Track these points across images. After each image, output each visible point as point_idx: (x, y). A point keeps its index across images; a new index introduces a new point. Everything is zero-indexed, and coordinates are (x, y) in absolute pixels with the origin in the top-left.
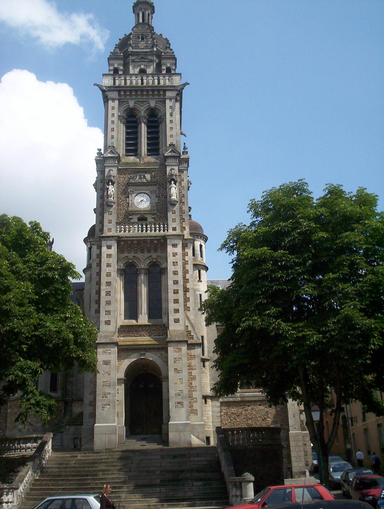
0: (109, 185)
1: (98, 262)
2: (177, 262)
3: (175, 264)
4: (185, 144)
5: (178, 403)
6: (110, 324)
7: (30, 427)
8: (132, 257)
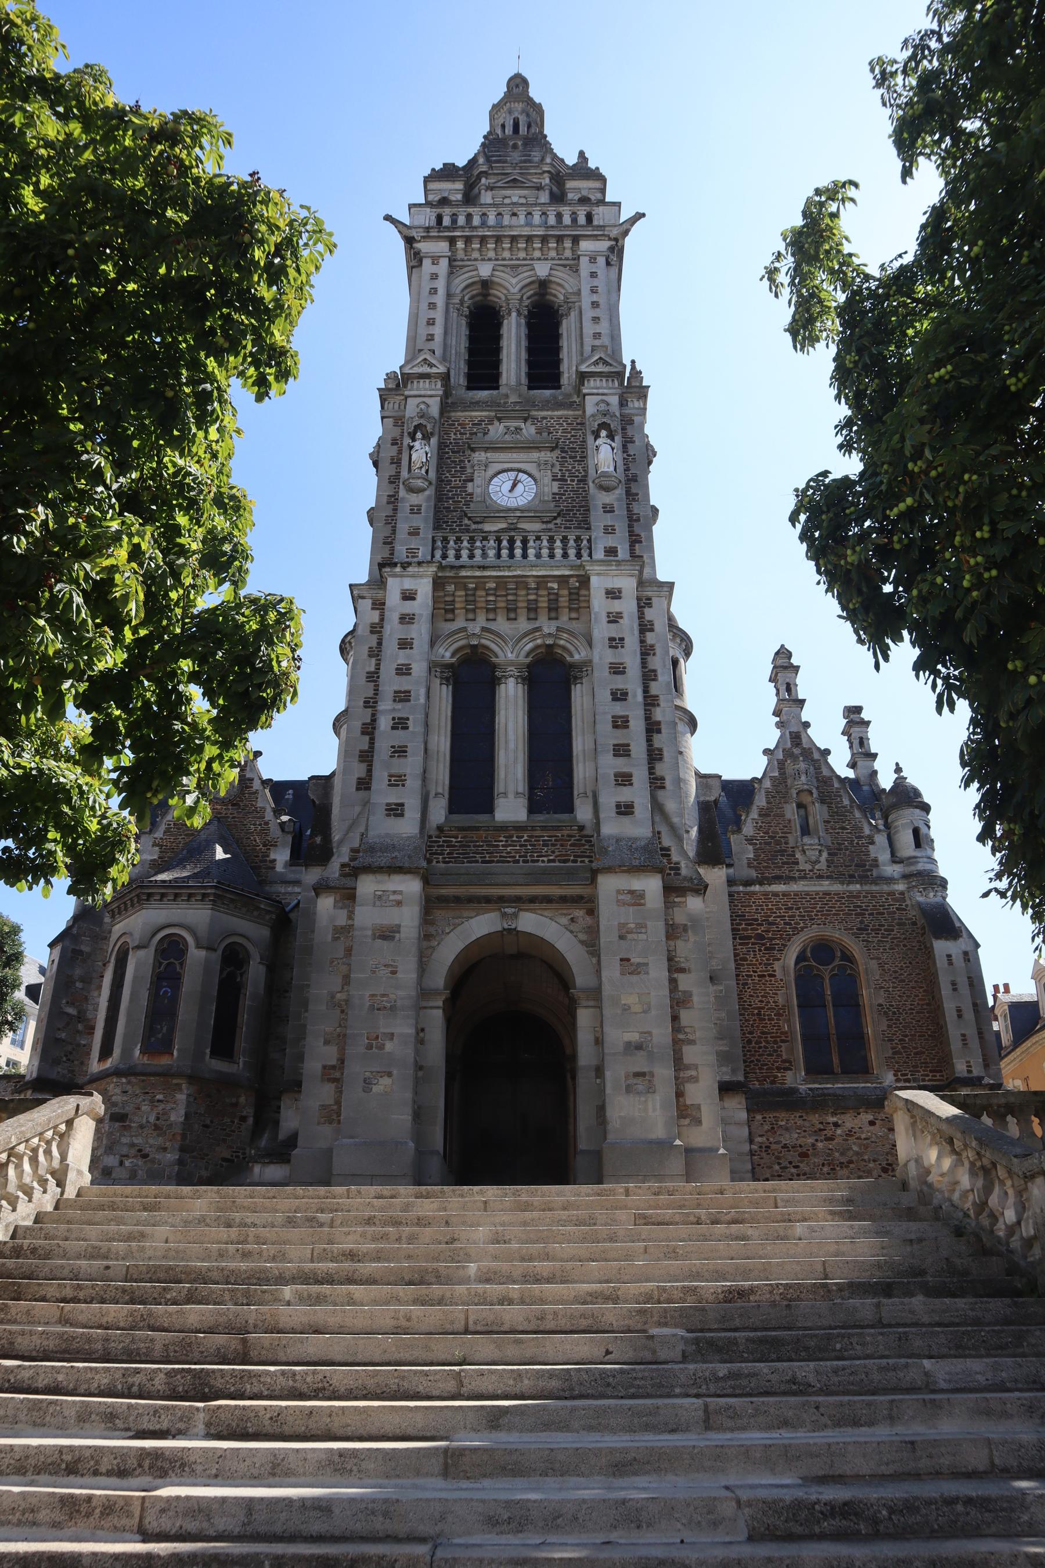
0: (414, 440)
1: (374, 644)
2: (622, 639)
3: (615, 643)
4: (633, 362)
5: (637, 1075)
6: (402, 815)
7: (140, 1162)
8: (477, 631)
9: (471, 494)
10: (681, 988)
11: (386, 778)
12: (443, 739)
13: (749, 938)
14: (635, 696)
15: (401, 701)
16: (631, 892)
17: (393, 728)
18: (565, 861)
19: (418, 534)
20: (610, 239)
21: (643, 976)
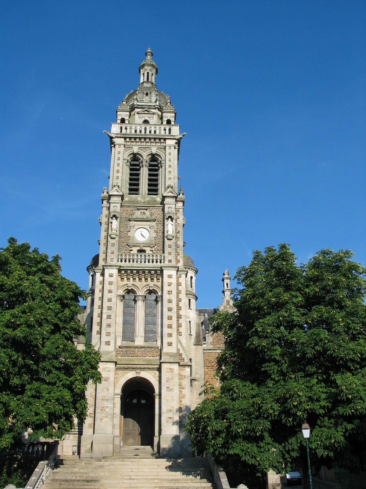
2: (171, 291)
3: (170, 292)
5: (170, 418)
9: (129, 236)
10: (183, 393)
11: (105, 334)
12: (120, 319)
13: (209, 366)
14: (174, 309)
15: (109, 310)
16: (170, 369)
17: (107, 318)
18: (154, 357)
19: (114, 253)
20: (176, 140)
21: (172, 392)
